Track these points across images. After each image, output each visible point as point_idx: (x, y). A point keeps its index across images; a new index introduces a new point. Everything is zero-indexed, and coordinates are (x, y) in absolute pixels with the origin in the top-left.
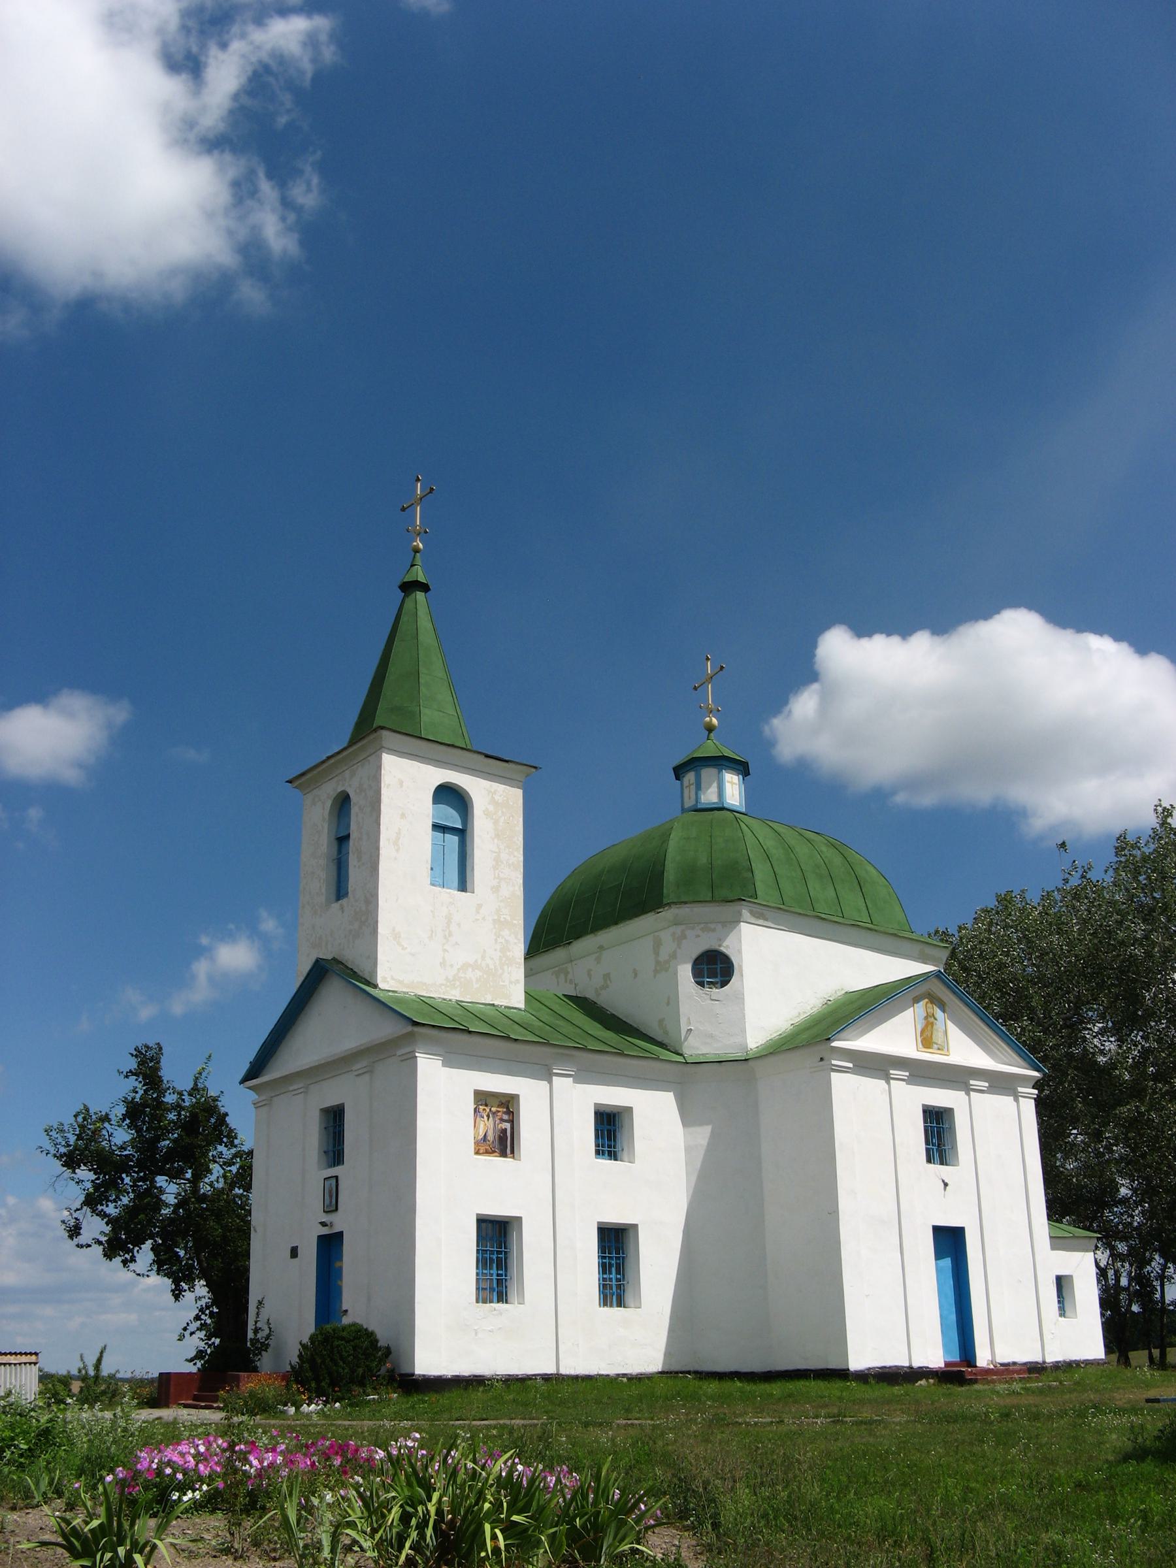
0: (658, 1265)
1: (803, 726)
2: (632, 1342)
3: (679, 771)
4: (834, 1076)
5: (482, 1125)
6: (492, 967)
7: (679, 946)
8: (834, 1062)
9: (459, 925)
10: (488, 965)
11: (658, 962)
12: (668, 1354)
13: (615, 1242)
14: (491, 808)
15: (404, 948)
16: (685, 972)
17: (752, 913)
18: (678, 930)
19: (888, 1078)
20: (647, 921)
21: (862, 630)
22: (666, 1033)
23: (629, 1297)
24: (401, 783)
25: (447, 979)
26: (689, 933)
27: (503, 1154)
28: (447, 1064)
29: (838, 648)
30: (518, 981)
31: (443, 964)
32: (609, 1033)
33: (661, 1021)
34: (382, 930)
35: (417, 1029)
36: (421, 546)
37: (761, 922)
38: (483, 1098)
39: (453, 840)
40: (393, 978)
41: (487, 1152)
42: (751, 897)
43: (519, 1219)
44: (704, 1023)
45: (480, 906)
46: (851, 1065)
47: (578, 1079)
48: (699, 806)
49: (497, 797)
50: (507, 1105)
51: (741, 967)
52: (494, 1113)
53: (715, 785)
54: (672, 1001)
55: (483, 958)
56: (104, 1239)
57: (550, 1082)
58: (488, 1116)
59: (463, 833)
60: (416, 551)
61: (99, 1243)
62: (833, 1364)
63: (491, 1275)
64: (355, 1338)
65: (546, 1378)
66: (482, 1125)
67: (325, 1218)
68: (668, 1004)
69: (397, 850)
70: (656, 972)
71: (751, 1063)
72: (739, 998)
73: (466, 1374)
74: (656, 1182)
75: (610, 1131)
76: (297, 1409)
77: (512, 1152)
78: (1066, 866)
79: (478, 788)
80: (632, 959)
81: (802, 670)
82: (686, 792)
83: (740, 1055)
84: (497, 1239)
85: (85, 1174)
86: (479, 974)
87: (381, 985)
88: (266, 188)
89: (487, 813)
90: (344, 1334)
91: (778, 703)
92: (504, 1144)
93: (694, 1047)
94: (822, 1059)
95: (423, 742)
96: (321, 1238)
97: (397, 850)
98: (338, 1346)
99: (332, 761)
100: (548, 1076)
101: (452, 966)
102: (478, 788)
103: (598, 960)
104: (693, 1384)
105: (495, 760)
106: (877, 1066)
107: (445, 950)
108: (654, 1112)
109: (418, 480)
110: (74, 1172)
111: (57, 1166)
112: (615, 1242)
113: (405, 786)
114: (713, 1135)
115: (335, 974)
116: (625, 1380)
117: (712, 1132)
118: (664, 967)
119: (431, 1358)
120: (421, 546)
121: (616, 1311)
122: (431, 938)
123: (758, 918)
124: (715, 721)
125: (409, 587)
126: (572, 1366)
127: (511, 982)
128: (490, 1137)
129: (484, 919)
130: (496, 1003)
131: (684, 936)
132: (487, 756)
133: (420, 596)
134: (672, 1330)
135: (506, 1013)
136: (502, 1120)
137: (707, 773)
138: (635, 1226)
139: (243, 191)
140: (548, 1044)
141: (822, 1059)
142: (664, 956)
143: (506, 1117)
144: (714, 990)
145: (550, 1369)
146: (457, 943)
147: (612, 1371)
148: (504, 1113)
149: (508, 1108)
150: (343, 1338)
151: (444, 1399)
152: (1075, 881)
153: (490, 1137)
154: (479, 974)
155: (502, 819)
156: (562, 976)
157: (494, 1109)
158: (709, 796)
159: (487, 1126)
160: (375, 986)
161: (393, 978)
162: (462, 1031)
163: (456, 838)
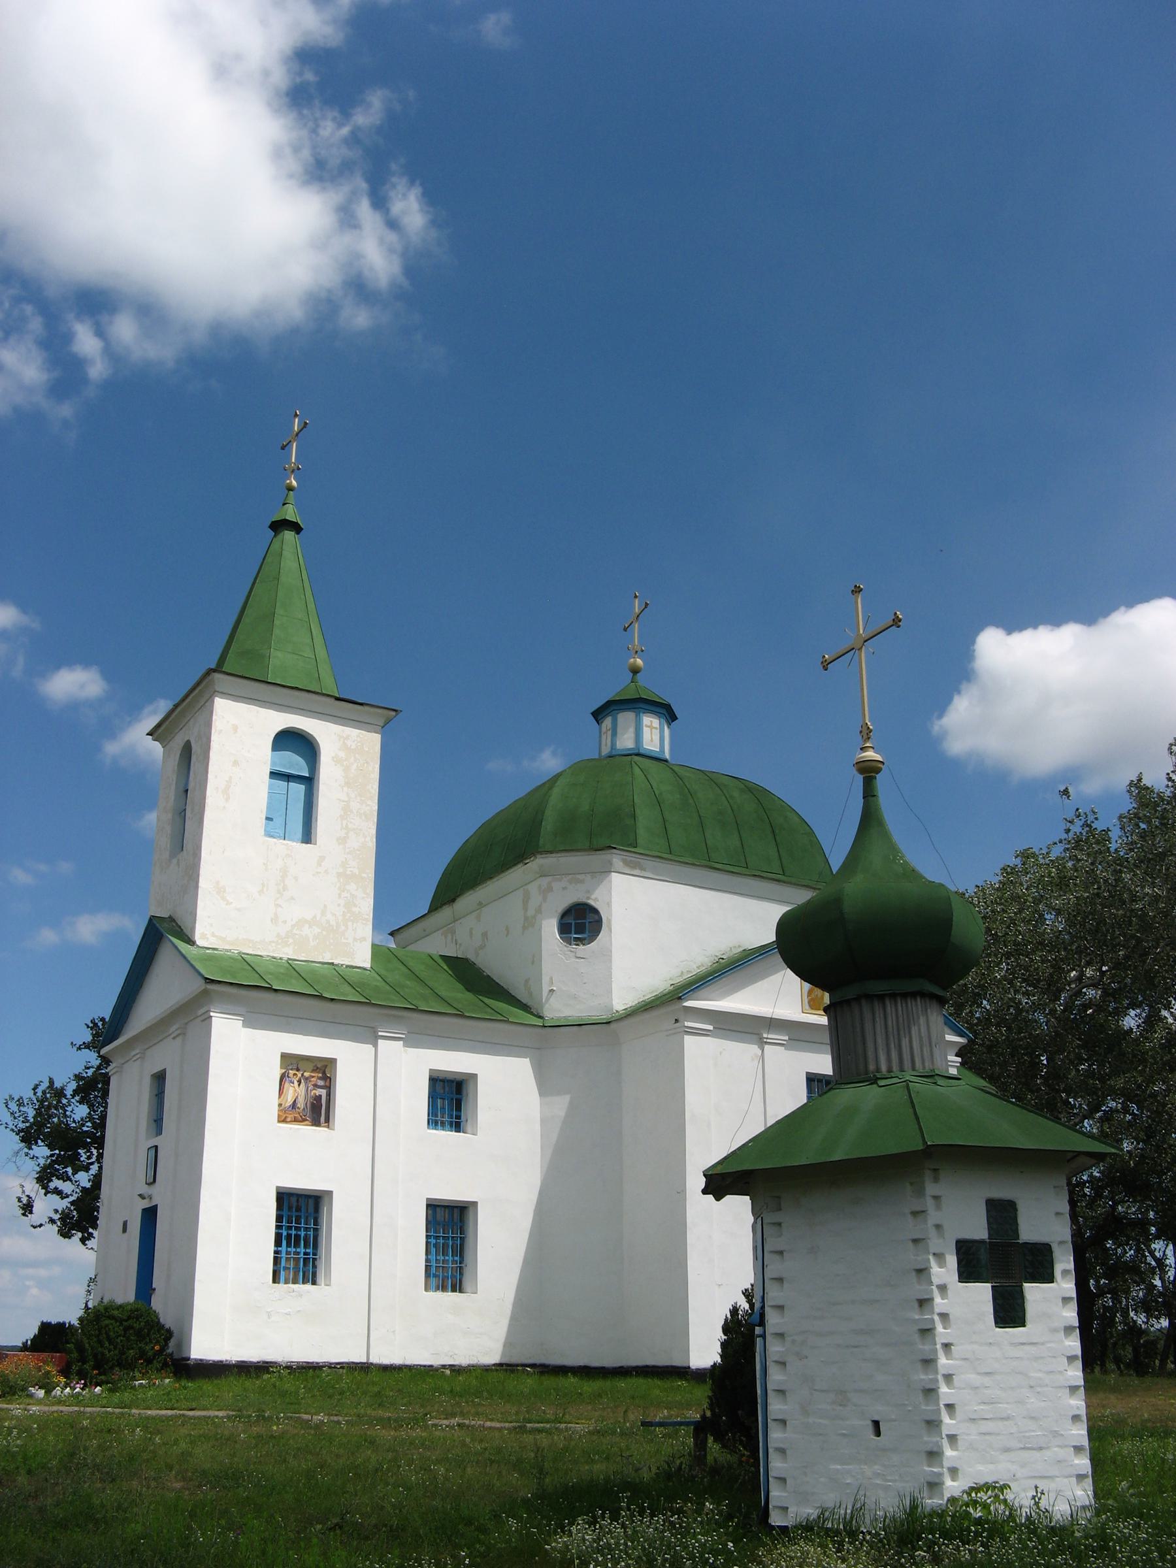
0: (500, 1250)
1: (964, 725)
2: (468, 1330)
3: (598, 715)
4: (688, 1039)
5: (291, 1090)
6: (333, 923)
7: (545, 899)
8: (686, 1024)
9: (296, 879)
10: (328, 922)
11: (526, 918)
12: (508, 1344)
13: (450, 1226)
14: (342, 754)
15: (228, 903)
16: (550, 928)
17: (626, 863)
18: (544, 882)
19: (762, 1043)
20: (517, 874)
21: (1013, 625)
22: (531, 994)
23: (467, 1284)
24: (235, 729)
25: (278, 935)
26: (556, 886)
27: (316, 1123)
28: (248, 1024)
29: (996, 649)
30: (364, 939)
31: (275, 920)
32: (481, 996)
33: (527, 981)
34: (203, 883)
35: (210, 987)
36: (294, 483)
37: (636, 872)
38: (291, 1062)
39: (299, 789)
40: (213, 935)
41: (295, 1120)
42: (630, 845)
43: (330, 1193)
44: (566, 981)
45: (322, 858)
46: (710, 1027)
47: (409, 1042)
48: (642, 751)
49: (349, 743)
50: (324, 1070)
51: (609, 921)
52: (306, 1079)
53: (632, 730)
54: (536, 960)
55: (323, 913)
56: (56, 1217)
57: (375, 1046)
58: (299, 1082)
59: (310, 782)
60: (290, 488)
61: (52, 1221)
62: (677, 1362)
63: (298, 1253)
64: (129, 1318)
65: (352, 1367)
66: (291, 1090)
67: (144, 1189)
68: (533, 963)
69: (227, 800)
70: (524, 928)
71: (613, 1026)
72: (607, 955)
73: (255, 1359)
74: (504, 1161)
75: (450, 1100)
76: (48, 1392)
77: (327, 1120)
78: (1070, 815)
79: (328, 734)
80: (513, 920)
81: (956, 669)
82: (604, 737)
83: (605, 1017)
84: (300, 1223)
85: (42, 1151)
86: (317, 930)
87: (199, 942)
88: (364, 209)
89: (337, 760)
90: (116, 1313)
91: (942, 705)
92: (318, 1112)
93: (556, 1009)
94: (677, 1021)
95: (257, 680)
96: (144, 1211)
97: (227, 800)
98: (107, 1326)
99: (179, 709)
100: (374, 1039)
101: (285, 922)
102: (328, 734)
103: (478, 918)
104: (530, 1382)
105: (346, 704)
106: (751, 1028)
107: (278, 906)
108: (504, 1081)
109: (296, 415)
110: (30, 1148)
111: (15, 1142)
112: (450, 1226)
113: (241, 733)
114: (572, 1108)
115: (162, 934)
116: (448, 1372)
117: (571, 1103)
118: (531, 924)
119: (208, 1342)
120: (294, 483)
121: (450, 1297)
122: (261, 892)
123: (634, 868)
124: (639, 662)
125: (279, 526)
126: (385, 1354)
127: (355, 940)
128: (301, 1104)
129: (326, 872)
130: (336, 962)
131: (550, 889)
132: (338, 699)
133: (289, 535)
134: (514, 1319)
135: (343, 975)
136: (316, 1086)
137: (626, 718)
138: (475, 1204)
139: (346, 218)
140: (370, 1004)
141: (677, 1021)
142: (531, 913)
143: (321, 1083)
144: (581, 947)
145: (358, 1357)
146: (292, 898)
147: (436, 1362)
148: (320, 1078)
149: (324, 1073)
150: (112, 1317)
151: (207, 1386)
152: (1076, 828)
153: (301, 1104)
154: (317, 930)
155: (354, 766)
156: (450, 936)
157: (307, 1074)
158: (626, 742)
159: (296, 1092)
160: (190, 942)
161: (213, 935)
162: (265, 990)
163: (303, 787)
